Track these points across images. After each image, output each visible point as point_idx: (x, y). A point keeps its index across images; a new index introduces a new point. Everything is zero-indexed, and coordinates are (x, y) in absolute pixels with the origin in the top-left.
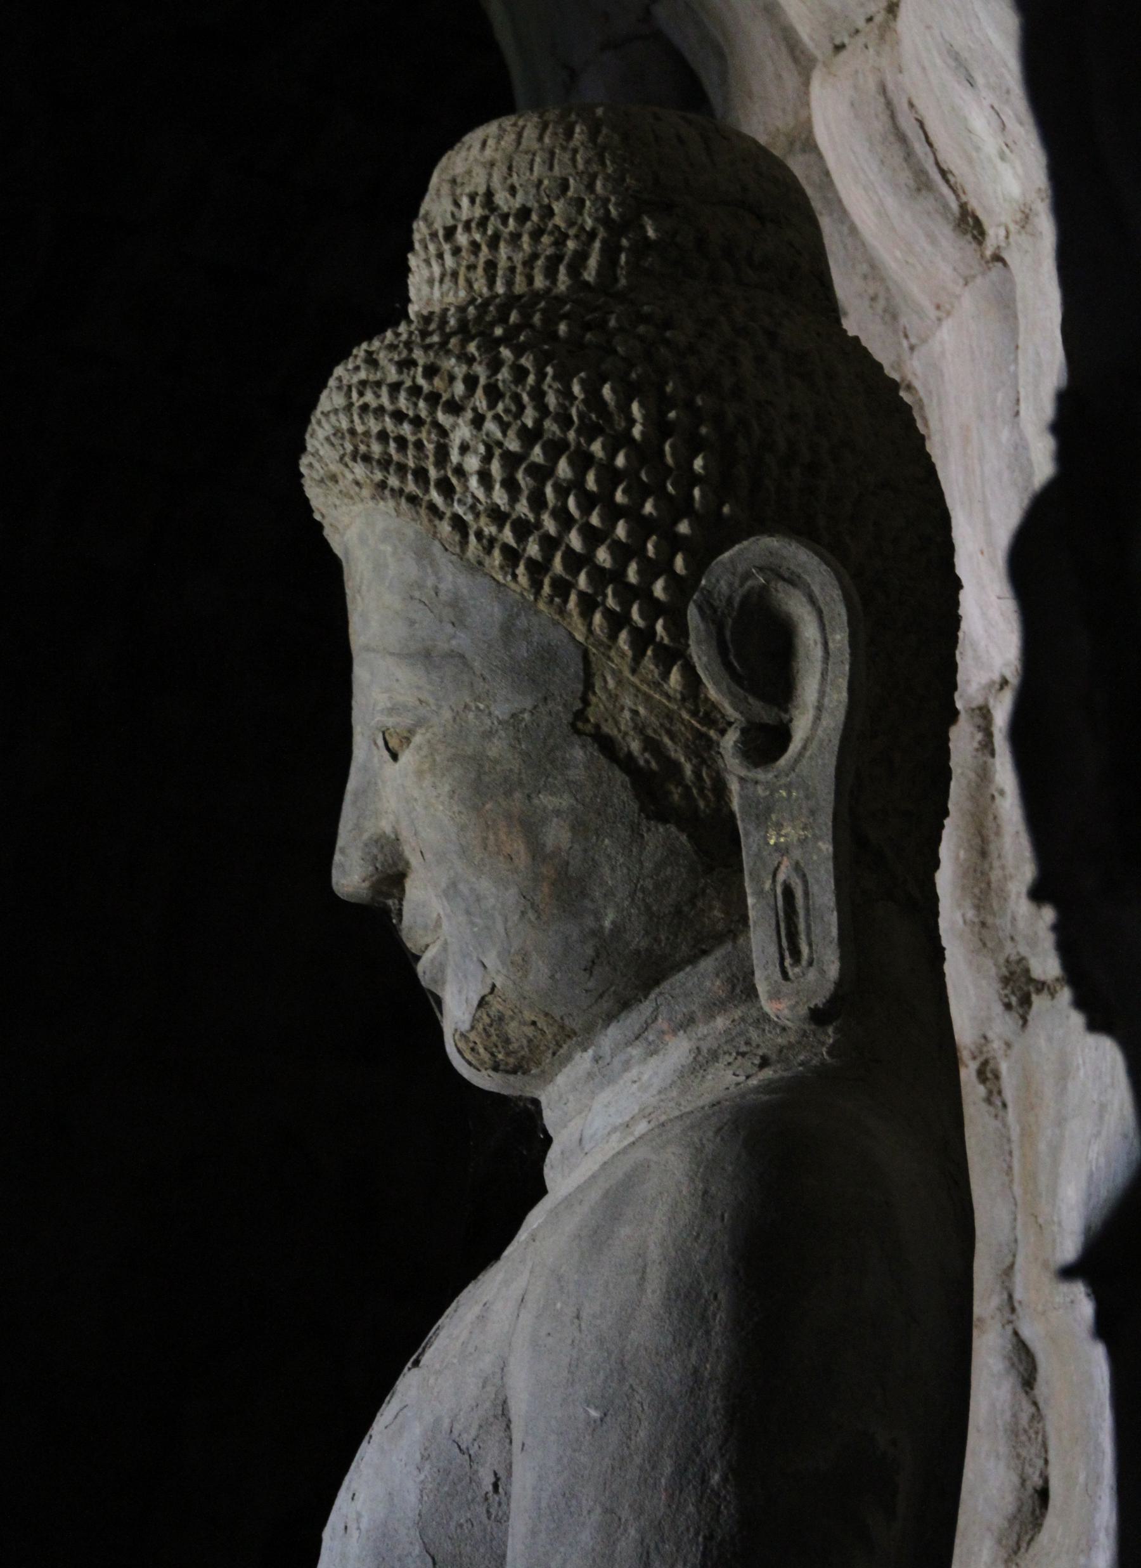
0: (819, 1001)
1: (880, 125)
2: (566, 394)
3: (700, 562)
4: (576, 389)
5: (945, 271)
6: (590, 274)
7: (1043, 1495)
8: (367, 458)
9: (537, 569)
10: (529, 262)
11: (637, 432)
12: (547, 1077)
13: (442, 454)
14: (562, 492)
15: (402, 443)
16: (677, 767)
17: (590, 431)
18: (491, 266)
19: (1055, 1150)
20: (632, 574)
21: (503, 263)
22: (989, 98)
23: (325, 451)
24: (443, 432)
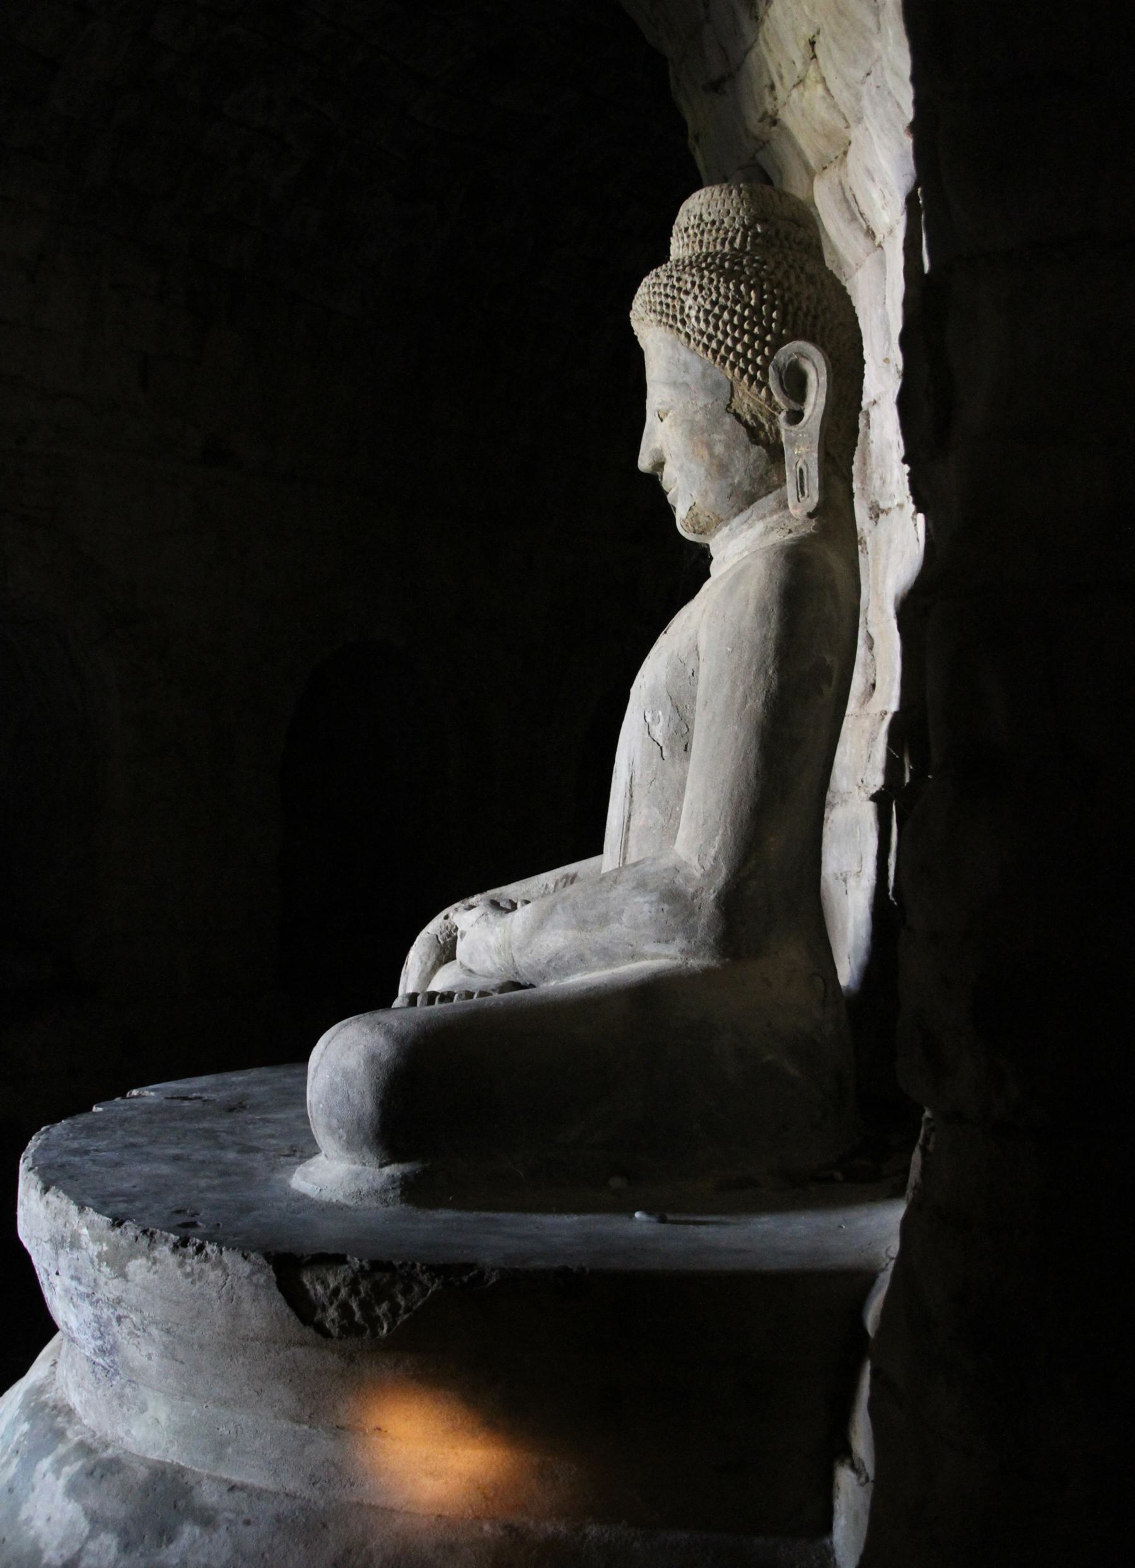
0: (811, 510)
1: (839, 196)
2: (728, 288)
3: (775, 348)
4: (731, 286)
5: (861, 251)
6: (737, 245)
7: (874, 686)
8: (655, 311)
9: (715, 352)
10: (715, 240)
11: (752, 303)
12: (712, 535)
13: (682, 309)
14: (725, 324)
15: (668, 306)
16: (763, 425)
17: (736, 302)
18: (701, 242)
19: (885, 568)
20: (749, 355)
21: (705, 241)
22: (880, 186)
23: (640, 309)
24: (683, 302)
